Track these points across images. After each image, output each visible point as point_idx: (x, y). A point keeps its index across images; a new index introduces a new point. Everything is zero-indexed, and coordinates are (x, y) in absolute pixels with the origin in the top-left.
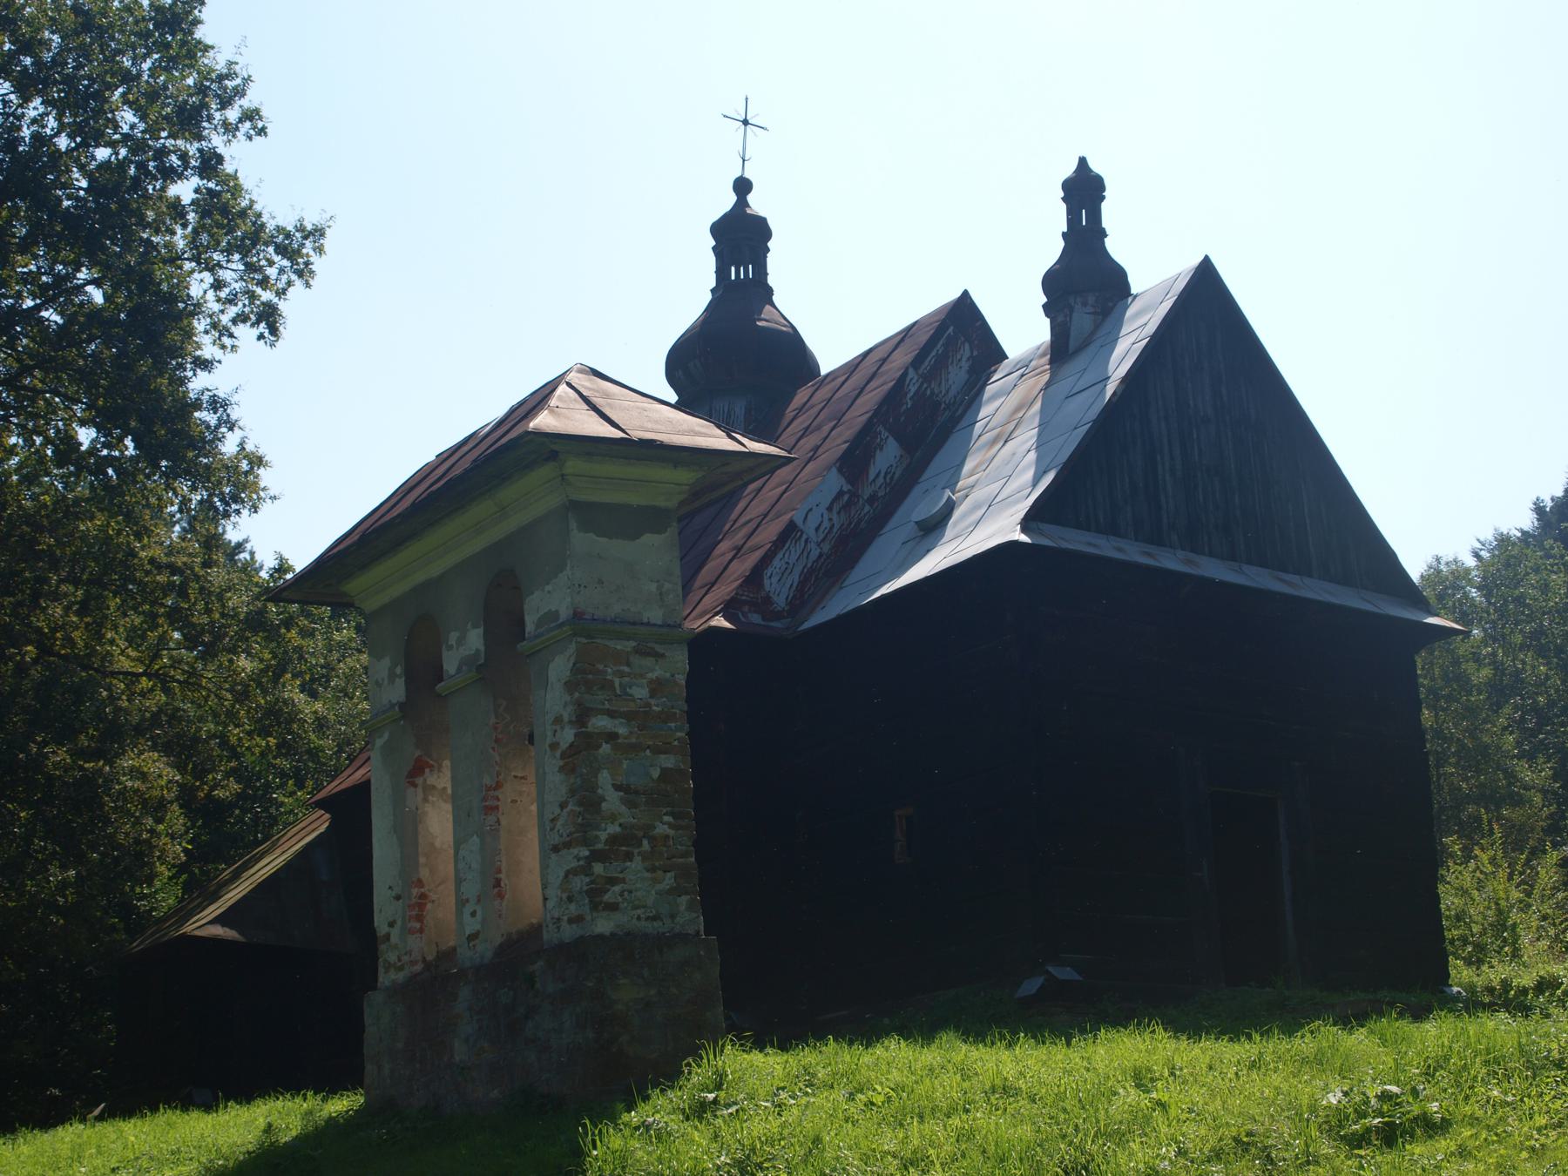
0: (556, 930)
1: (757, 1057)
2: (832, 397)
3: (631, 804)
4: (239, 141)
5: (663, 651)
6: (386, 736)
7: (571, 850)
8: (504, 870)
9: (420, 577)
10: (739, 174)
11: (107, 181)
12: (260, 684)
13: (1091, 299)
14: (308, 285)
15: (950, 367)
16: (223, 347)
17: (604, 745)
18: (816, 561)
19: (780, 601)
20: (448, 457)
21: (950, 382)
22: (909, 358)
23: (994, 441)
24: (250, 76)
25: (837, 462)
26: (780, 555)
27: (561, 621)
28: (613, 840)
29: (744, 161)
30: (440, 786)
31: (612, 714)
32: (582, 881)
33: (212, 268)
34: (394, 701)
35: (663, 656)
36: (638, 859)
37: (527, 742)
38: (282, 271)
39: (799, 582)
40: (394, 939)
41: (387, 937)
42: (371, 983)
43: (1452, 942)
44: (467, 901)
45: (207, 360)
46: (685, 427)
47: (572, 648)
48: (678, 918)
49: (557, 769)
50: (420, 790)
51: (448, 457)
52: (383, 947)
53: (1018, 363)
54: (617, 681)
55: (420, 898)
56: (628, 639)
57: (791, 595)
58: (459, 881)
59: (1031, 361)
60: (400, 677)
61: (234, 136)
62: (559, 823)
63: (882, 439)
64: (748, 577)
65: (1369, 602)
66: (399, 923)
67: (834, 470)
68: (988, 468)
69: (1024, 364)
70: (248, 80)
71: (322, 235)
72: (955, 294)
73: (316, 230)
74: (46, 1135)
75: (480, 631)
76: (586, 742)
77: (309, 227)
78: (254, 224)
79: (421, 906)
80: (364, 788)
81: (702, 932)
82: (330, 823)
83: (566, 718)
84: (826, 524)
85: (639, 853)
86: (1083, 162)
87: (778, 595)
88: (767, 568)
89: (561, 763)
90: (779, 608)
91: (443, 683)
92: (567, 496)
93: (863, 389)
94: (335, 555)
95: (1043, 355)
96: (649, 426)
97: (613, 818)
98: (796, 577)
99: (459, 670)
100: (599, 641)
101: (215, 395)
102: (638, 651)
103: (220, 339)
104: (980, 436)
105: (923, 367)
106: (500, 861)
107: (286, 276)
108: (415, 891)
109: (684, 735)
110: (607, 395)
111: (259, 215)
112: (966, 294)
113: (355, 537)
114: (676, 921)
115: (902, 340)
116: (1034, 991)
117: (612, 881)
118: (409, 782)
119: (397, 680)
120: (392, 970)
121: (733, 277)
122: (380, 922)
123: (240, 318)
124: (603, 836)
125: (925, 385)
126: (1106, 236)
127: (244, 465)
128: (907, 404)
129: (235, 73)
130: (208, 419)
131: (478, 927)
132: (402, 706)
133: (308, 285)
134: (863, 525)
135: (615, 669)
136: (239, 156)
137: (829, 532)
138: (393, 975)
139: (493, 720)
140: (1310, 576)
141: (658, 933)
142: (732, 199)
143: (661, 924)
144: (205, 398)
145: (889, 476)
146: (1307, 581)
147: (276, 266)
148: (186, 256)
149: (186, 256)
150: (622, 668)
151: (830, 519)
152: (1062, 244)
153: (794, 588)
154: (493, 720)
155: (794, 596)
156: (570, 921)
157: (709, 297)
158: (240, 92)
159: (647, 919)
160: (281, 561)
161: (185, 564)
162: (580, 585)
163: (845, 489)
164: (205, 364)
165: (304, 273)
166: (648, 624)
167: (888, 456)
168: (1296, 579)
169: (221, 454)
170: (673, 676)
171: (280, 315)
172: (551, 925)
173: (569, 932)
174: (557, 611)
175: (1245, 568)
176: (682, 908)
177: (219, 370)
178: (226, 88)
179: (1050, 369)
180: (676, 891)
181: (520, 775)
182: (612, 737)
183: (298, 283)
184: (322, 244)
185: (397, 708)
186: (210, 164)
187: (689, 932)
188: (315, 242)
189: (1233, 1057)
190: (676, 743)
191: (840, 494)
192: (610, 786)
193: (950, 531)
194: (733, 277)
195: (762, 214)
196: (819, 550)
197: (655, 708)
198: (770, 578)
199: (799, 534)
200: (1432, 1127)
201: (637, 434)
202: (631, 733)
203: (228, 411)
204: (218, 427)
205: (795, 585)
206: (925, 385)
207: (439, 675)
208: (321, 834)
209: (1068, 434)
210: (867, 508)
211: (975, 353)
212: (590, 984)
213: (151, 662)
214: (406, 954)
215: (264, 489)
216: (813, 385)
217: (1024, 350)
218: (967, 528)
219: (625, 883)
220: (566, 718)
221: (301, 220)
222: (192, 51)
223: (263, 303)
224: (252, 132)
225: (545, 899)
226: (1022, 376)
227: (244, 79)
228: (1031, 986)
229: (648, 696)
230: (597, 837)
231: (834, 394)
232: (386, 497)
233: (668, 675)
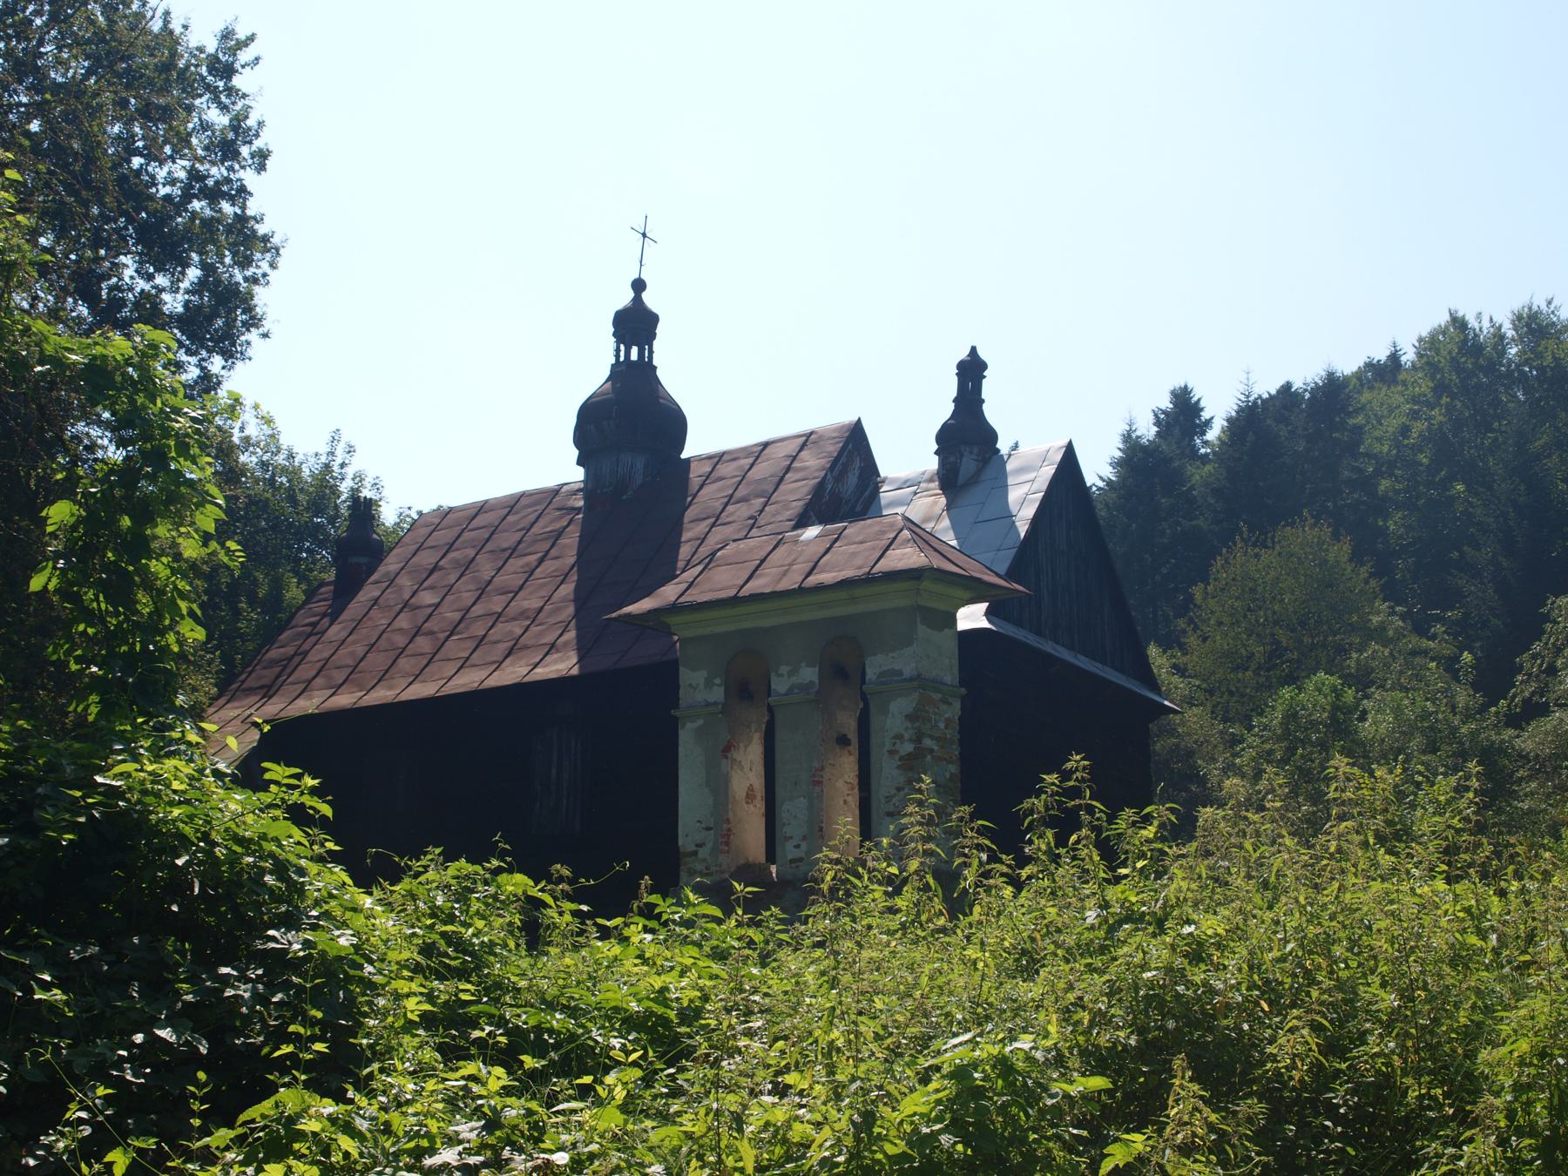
43: (941, 913)
72: (854, 418)
79: (729, 836)
83: (907, 736)
86: (974, 349)
95: (931, 480)
122: (685, 841)
142: (629, 295)
168: (1100, 666)
182: (931, 751)
220: (907, 736)
226: (916, 493)
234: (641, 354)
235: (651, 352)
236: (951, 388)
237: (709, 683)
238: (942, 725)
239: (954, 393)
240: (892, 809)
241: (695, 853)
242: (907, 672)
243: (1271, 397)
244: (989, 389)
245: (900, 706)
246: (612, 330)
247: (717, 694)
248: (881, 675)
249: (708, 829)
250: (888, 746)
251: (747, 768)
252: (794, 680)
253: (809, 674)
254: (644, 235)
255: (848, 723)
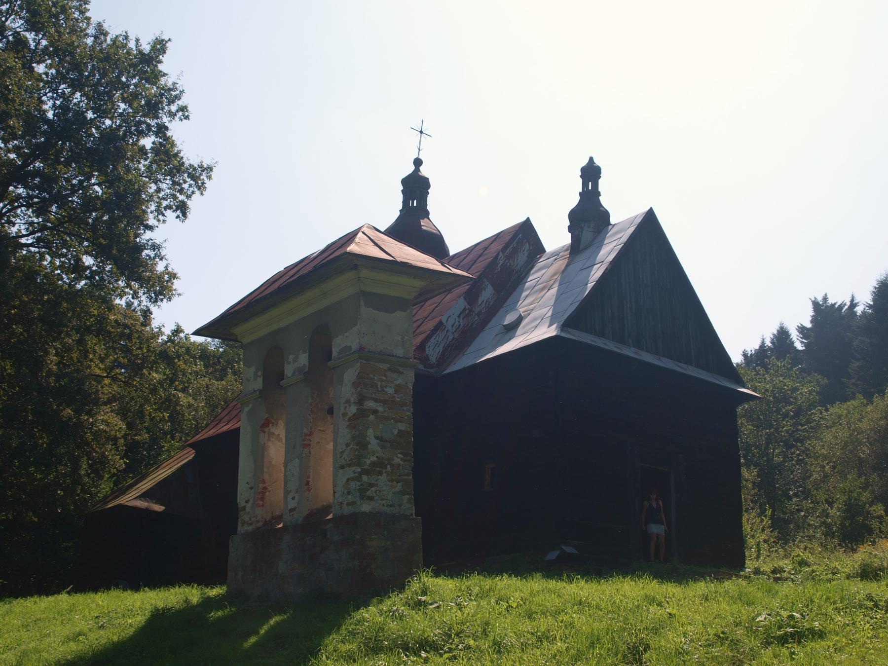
0: (340, 509)
1: (440, 581)
2: (459, 264)
3: (383, 447)
4: (175, 121)
5: (402, 371)
6: (250, 406)
7: (351, 468)
8: (311, 477)
9: (274, 327)
10: (417, 157)
11: (110, 136)
12: (162, 386)
14: (202, 194)
15: (519, 254)
16: (159, 220)
17: (371, 416)
18: (451, 341)
19: (433, 359)
20: (292, 269)
21: (519, 261)
22: (500, 247)
23: (542, 289)
24: (183, 90)
25: (464, 294)
26: (434, 337)
27: (352, 351)
28: (373, 464)
29: (419, 150)
30: (277, 433)
31: (376, 400)
32: (356, 484)
33: (156, 182)
34: (256, 389)
35: (402, 373)
36: (385, 475)
37: (326, 413)
38: (190, 186)
39: (443, 351)
40: (248, 509)
41: (244, 508)
42: (234, 531)
44: (291, 491)
45: (151, 226)
46: (421, 259)
47: (359, 364)
48: (402, 507)
49: (346, 426)
50: (266, 434)
51: (292, 269)
52: (241, 513)
53: (553, 254)
54: (379, 384)
55: (263, 489)
57: (439, 356)
58: (286, 481)
59: (560, 253)
60: (260, 377)
61: (173, 119)
62: (345, 454)
63: (485, 285)
64: (418, 347)
65: (717, 379)
66: (251, 501)
67: (462, 298)
68: (541, 301)
69: (556, 254)
70: (182, 92)
71: (211, 170)
73: (208, 168)
74: (136, 594)
75: (306, 355)
76: (362, 413)
77: (205, 166)
78: (179, 162)
79: (264, 493)
80: (238, 429)
81: (414, 515)
82: (195, 455)
83: (352, 400)
84: (457, 324)
85: (385, 472)
86: (591, 159)
87: (432, 356)
88: (428, 342)
89: (348, 423)
90: (432, 363)
91: (284, 381)
92: (360, 288)
93: (476, 261)
94: (230, 314)
95: (566, 250)
96: (404, 256)
97: (373, 453)
98: (441, 348)
99: (293, 374)
100: (372, 363)
101: (154, 243)
103: (157, 216)
104: (534, 287)
105: (506, 252)
106: (310, 472)
107: (192, 189)
108: (261, 485)
109: (410, 414)
110: (382, 240)
111: (182, 158)
112: (528, 219)
113: (245, 304)
114: (401, 508)
115: (495, 239)
116: (554, 558)
117: (371, 485)
118: (261, 430)
119: (258, 378)
120: (246, 525)
121: (415, 201)
122: (241, 500)
123: (169, 207)
124: (368, 462)
125: (507, 261)
126: (600, 195)
127: (166, 277)
128: (498, 269)
129: (176, 88)
130: (150, 254)
131: (296, 505)
132: (260, 391)
133: (202, 194)
134: (474, 326)
135: (379, 377)
136: (176, 129)
137: (458, 328)
138: (246, 528)
139: (310, 401)
140: (691, 365)
141: (393, 513)
142: (413, 168)
143: (394, 508)
144: (150, 243)
145: (488, 303)
146: (689, 367)
147: (188, 183)
148: (144, 175)
149: (144, 175)
150: (382, 377)
151: (459, 322)
152: (579, 198)
153: (440, 354)
154: (310, 401)
155: (440, 358)
156: (348, 504)
157: (398, 214)
158: (178, 97)
159: (388, 506)
160: (178, 327)
161: (132, 324)
162: (364, 334)
163: (467, 307)
164: (151, 228)
165: (201, 188)
166: (396, 356)
167: (487, 294)
168: (685, 366)
169: (156, 271)
170: (406, 383)
171: (188, 207)
172: (337, 506)
173: (347, 510)
174: (351, 346)
175: (662, 358)
176: (405, 501)
177: (156, 230)
178: (171, 95)
179: (569, 257)
181: (322, 429)
182: (375, 412)
183: (197, 192)
184: (211, 175)
185: (258, 392)
186: (162, 130)
187: (408, 514)
188: (207, 173)
190: (406, 418)
191: (464, 310)
192: (373, 437)
193: (520, 331)
194: (415, 201)
195: (427, 176)
196: (452, 336)
197: (397, 399)
198: (429, 347)
199: (444, 327)
200: (821, 635)
201: (399, 259)
202: (384, 411)
203: (160, 251)
204: (154, 258)
205: (440, 352)
206: (507, 261)
207: (282, 376)
208: (190, 460)
209: (582, 287)
210: (477, 318)
211: (531, 248)
212: (358, 537)
213: (111, 371)
214: (254, 517)
215: (175, 290)
216: (448, 259)
217: (557, 247)
218: (531, 329)
219: (377, 487)
220: (352, 400)
221: (202, 162)
222: (155, 76)
223: (180, 201)
224: (182, 117)
225: (334, 492)
226: (556, 259)
227: (180, 91)
228: (553, 555)
229: (394, 392)
230: (365, 462)
231: (460, 263)
232: (259, 286)
233: (404, 383)
236: (577, 185)
244: (604, 185)
250: (342, 411)
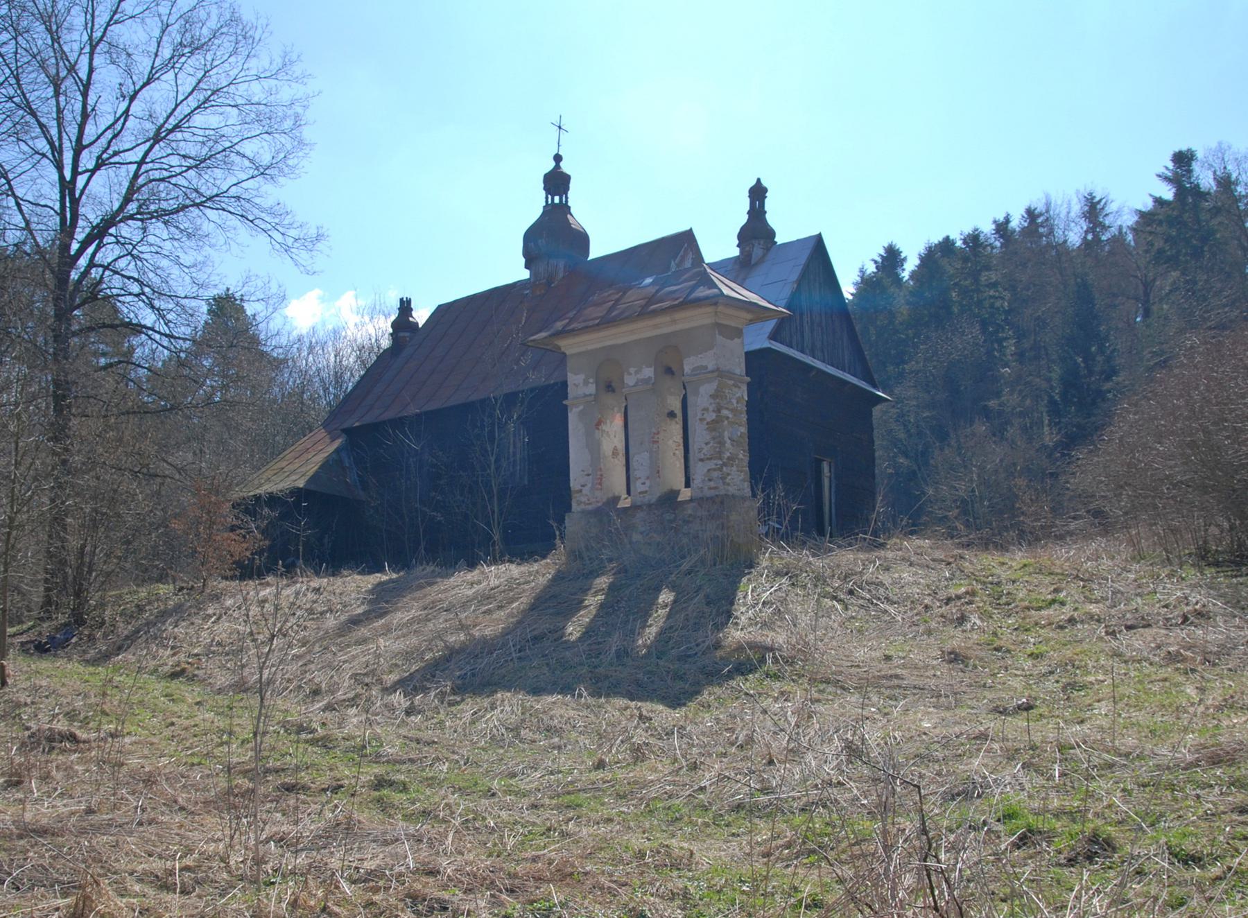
13: (762, 242)
56: (730, 379)
86: (759, 180)
102: (734, 385)
108: (599, 473)
112: (691, 229)
117: (728, 474)
122: (574, 484)
142: (553, 164)
180: (744, 480)
189: (700, 588)
195: (568, 173)
220: (711, 409)
234: (561, 200)
235: (567, 198)
237: (586, 383)
238: (734, 401)
239: (748, 208)
240: (702, 457)
241: (581, 491)
242: (710, 367)
243: (940, 243)
244: (769, 204)
245: (707, 389)
246: (543, 185)
247: (591, 389)
248: (694, 369)
249: (588, 475)
250: (699, 416)
251: (612, 436)
252: (638, 376)
253: (648, 372)
254: (560, 127)
255: (675, 404)
